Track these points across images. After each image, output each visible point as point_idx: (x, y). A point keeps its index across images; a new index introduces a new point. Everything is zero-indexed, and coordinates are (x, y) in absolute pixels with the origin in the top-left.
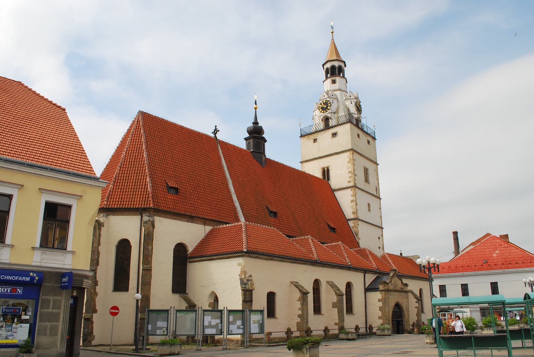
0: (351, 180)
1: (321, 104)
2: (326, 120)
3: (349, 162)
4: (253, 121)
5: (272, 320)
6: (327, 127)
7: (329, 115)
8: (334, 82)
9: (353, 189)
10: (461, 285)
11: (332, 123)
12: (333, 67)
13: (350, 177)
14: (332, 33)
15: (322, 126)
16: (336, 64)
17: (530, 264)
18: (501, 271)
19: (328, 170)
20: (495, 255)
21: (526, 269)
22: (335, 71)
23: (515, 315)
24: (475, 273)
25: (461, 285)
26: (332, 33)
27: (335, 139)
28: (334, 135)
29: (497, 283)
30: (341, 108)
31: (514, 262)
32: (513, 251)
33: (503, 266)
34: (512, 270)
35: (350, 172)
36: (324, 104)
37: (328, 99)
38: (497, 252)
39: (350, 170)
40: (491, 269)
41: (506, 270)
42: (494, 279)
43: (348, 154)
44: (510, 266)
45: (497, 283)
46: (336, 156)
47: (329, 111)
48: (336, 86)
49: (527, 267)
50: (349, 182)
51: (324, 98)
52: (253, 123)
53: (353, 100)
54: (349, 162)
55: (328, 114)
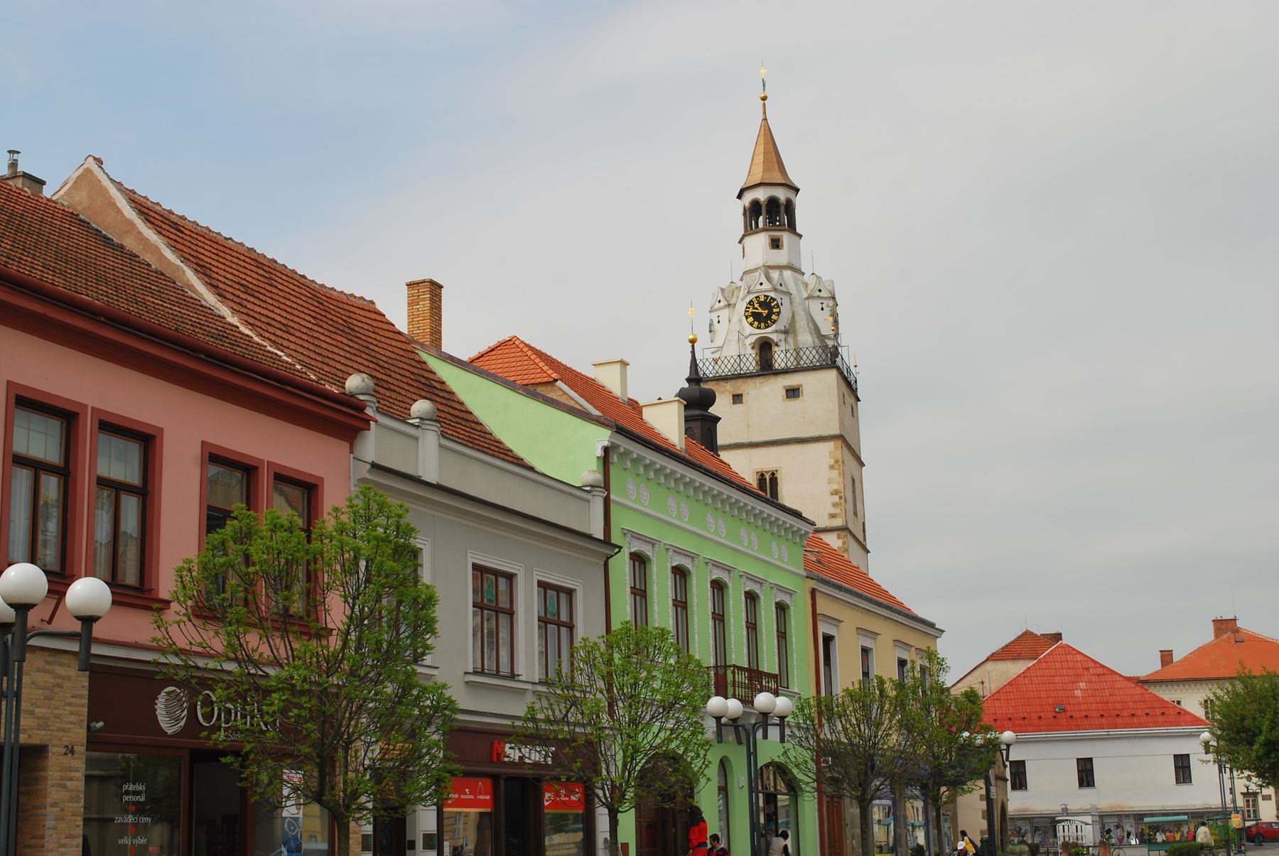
0: (837, 511)
1: (751, 303)
2: (765, 347)
3: (832, 467)
4: (687, 375)
5: (1018, 793)
6: (766, 367)
7: (775, 337)
8: (776, 244)
9: (843, 534)
10: (1078, 760)
11: (780, 360)
12: (773, 201)
13: (835, 505)
14: (764, 99)
15: (751, 364)
16: (782, 194)
17: (1162, 719)
18: (1102, 732)
19: (774, 480)
20: (1078, 693)
21: (1157, 730)
22: (772, 214)
23: (1129, 834)
24: (1043, 735)
25: (1078, 760)
26: (764, 99)
27: (794, 404)
28: (793, 393)
29: (1023, 762)
30: (801, 322)
31: (1125, 713)
32: (1118, 685)
33: (1104, 721)
34: (1125, 731)
35: (835, 492)
36: (761, 304)
37: (772, 295)
38: (1082, 685)
39: (835, 487)
40: (1078, 727)
41: (1113, 732)
42: (1084, 751)
43: (830, 446)
44: (1119, 720)
45: (1023, 762)
46: (799, 447)
47: (773, 328)
48: (781, 257)
49: (1157, 725)
50: (833, 516)
51: (759, 287)
52: (688, 380)
53: (826, 302)
54: (832, 467)
55: (769, 332)
